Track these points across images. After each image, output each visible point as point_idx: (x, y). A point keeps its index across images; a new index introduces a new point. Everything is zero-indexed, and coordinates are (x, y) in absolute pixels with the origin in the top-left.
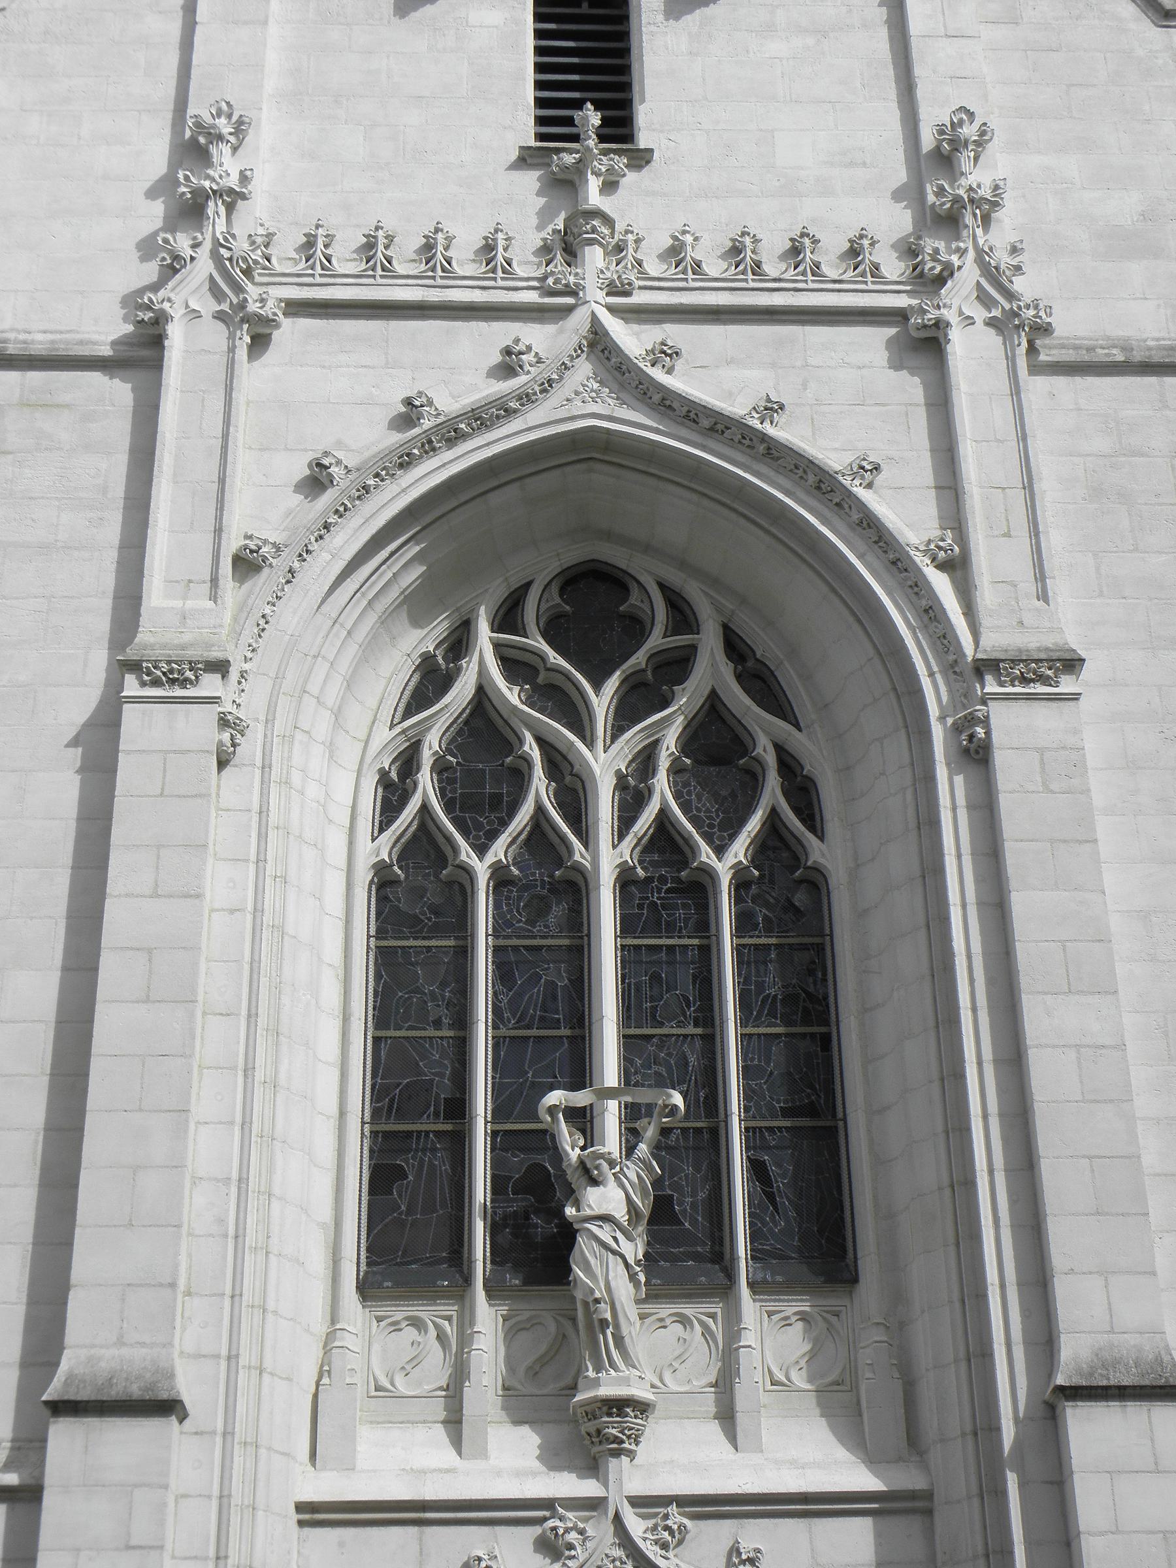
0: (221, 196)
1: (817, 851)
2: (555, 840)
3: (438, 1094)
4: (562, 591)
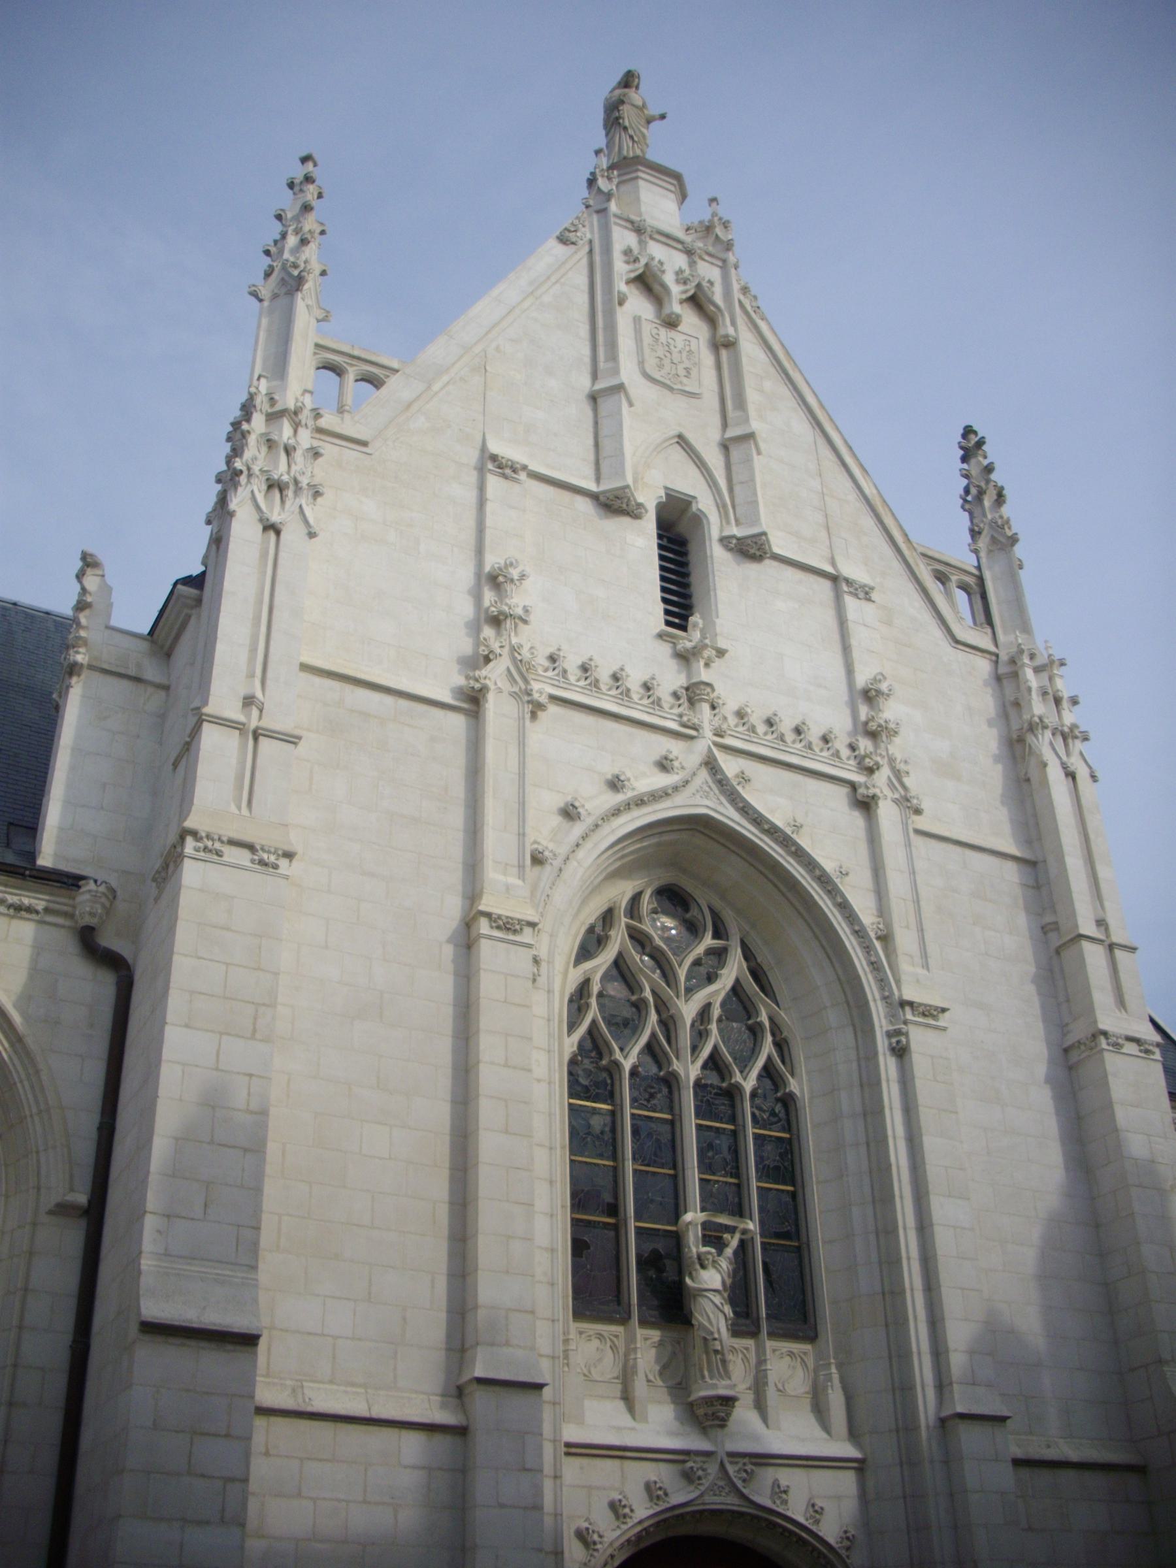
0: (514, 618)
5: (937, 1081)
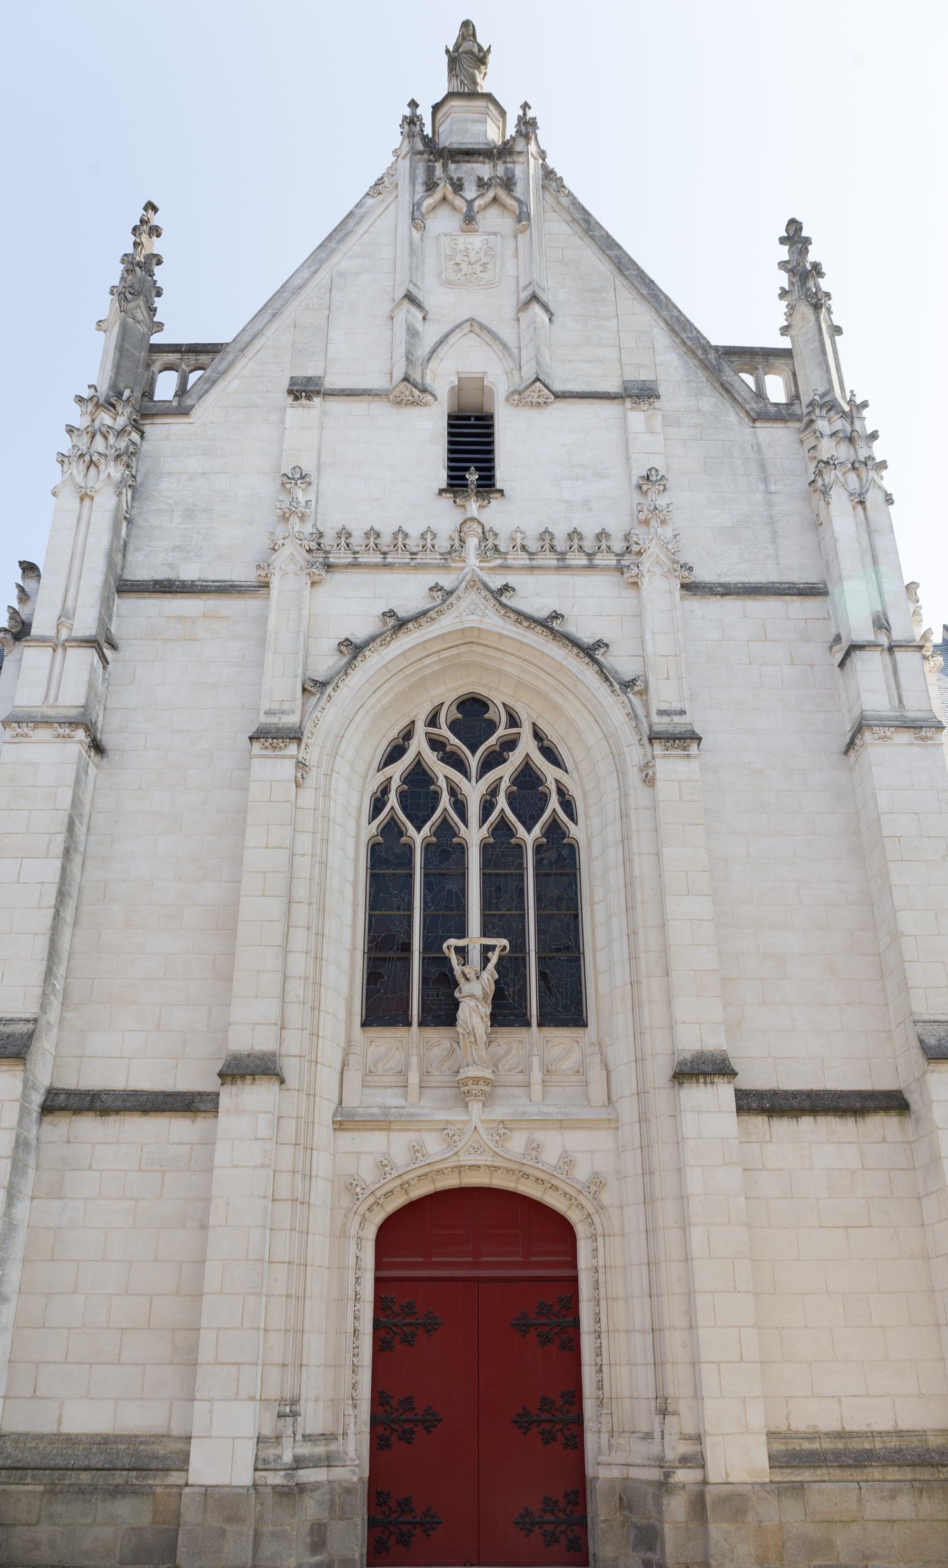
1: (574, 831)
2: (453, 825)
3: (398, 941)
4: (458, 708)
5: (684, 801)
